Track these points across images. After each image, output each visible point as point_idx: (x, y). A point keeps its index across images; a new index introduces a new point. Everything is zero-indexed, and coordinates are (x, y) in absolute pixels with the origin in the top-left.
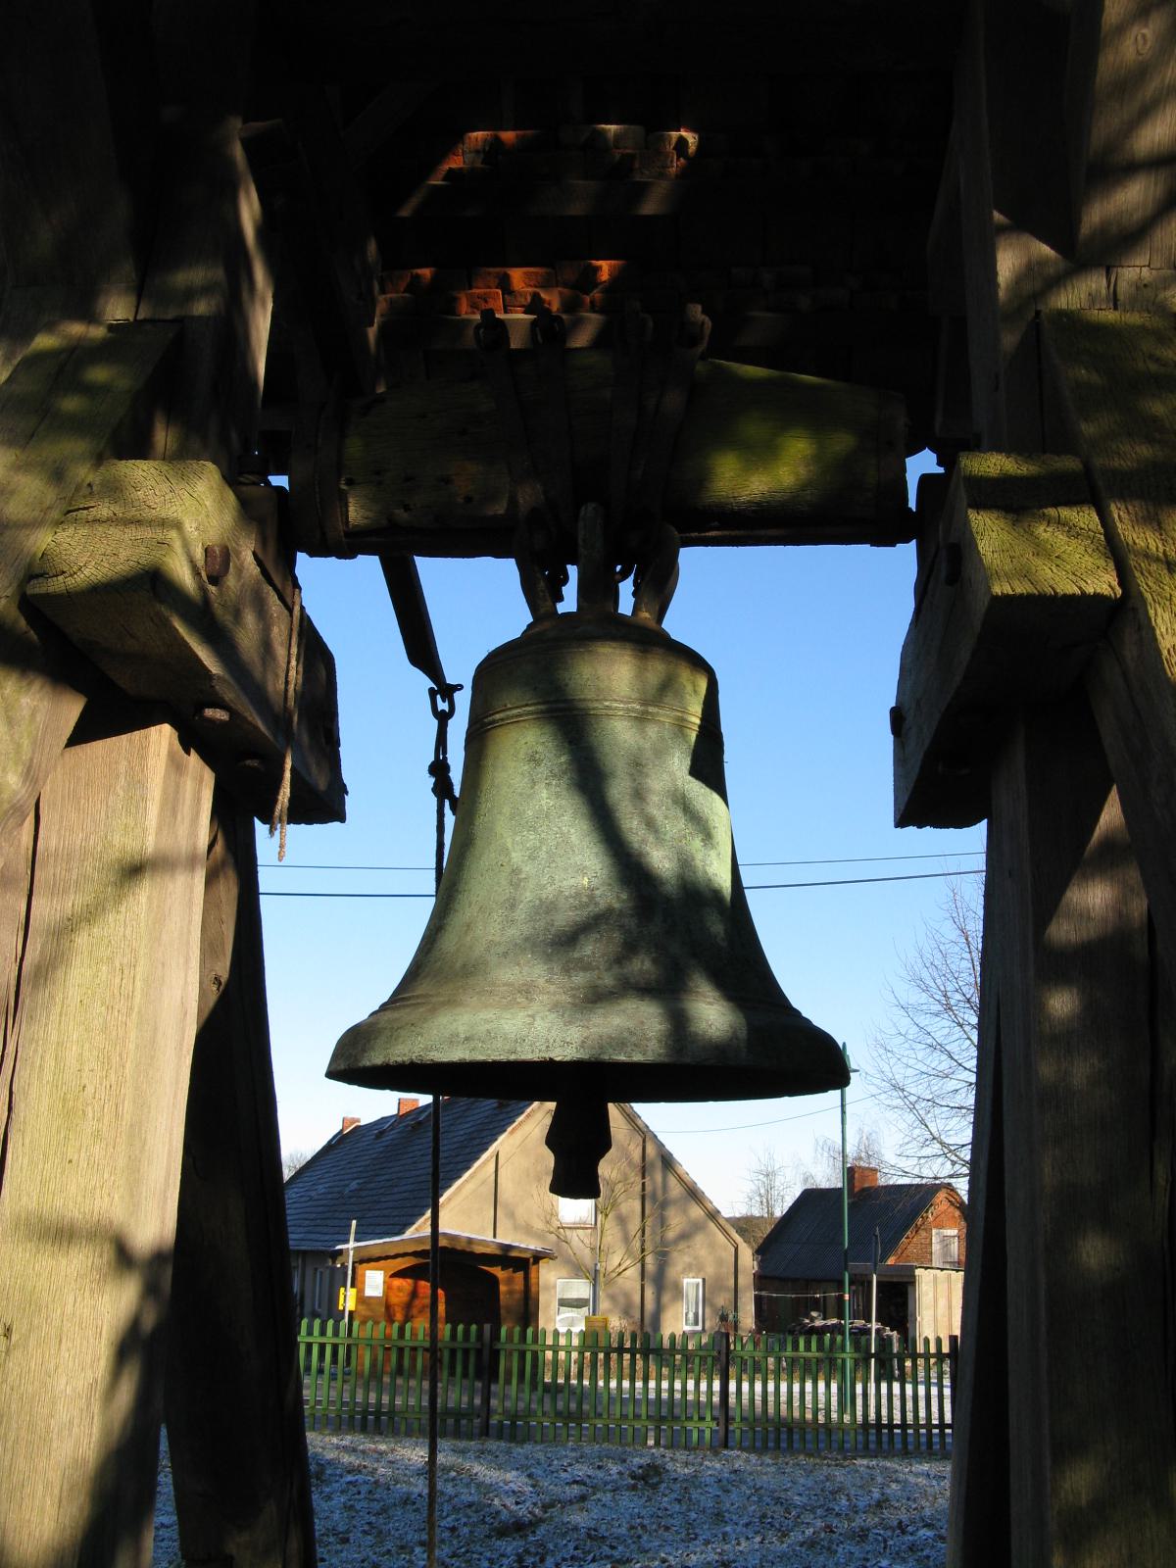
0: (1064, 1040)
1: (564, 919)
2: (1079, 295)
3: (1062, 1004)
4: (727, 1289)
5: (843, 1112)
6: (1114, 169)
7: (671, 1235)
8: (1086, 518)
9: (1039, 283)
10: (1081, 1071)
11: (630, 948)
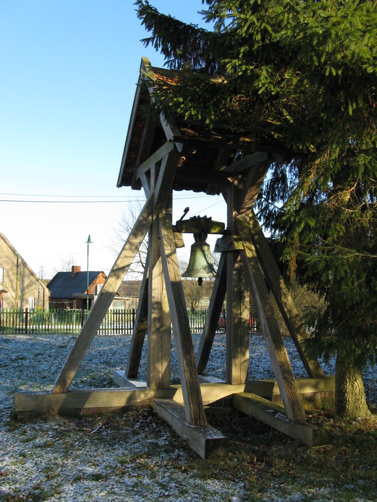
0: (234, 275)
1: (205, 267)
2: (239, 217)
3: (235, 272)
4: (41, 301)
5: (88, 253)
6: (243, 208)
7: (25, 285)
8: (241, 242)
9: (236, 215)
10: (235, 277)
11: (209, 269)
